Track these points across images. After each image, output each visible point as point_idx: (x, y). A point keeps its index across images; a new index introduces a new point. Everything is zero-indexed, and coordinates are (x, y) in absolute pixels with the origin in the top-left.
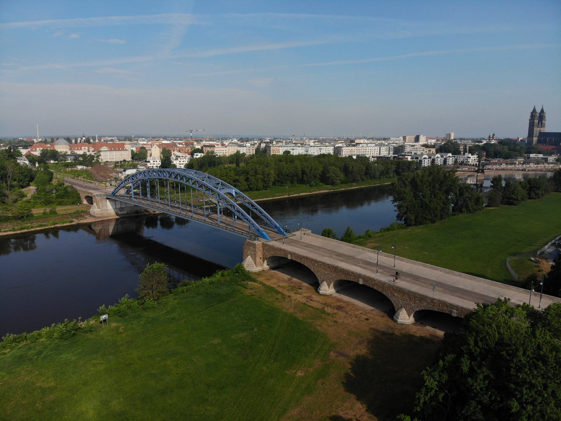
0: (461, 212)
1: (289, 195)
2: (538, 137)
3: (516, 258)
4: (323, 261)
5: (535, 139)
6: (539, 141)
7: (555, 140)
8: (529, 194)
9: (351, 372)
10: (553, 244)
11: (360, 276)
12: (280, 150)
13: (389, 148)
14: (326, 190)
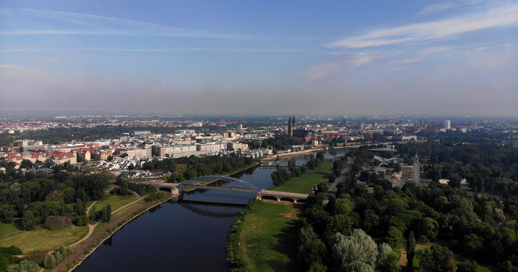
2: (293, 132)
4: (90, 235)
5: (292, 133)
6: (294, 135)
8: (302, 172)
10: (313, 188)
11: (286, 196)
12: (166, 150)
13: (225, 145)
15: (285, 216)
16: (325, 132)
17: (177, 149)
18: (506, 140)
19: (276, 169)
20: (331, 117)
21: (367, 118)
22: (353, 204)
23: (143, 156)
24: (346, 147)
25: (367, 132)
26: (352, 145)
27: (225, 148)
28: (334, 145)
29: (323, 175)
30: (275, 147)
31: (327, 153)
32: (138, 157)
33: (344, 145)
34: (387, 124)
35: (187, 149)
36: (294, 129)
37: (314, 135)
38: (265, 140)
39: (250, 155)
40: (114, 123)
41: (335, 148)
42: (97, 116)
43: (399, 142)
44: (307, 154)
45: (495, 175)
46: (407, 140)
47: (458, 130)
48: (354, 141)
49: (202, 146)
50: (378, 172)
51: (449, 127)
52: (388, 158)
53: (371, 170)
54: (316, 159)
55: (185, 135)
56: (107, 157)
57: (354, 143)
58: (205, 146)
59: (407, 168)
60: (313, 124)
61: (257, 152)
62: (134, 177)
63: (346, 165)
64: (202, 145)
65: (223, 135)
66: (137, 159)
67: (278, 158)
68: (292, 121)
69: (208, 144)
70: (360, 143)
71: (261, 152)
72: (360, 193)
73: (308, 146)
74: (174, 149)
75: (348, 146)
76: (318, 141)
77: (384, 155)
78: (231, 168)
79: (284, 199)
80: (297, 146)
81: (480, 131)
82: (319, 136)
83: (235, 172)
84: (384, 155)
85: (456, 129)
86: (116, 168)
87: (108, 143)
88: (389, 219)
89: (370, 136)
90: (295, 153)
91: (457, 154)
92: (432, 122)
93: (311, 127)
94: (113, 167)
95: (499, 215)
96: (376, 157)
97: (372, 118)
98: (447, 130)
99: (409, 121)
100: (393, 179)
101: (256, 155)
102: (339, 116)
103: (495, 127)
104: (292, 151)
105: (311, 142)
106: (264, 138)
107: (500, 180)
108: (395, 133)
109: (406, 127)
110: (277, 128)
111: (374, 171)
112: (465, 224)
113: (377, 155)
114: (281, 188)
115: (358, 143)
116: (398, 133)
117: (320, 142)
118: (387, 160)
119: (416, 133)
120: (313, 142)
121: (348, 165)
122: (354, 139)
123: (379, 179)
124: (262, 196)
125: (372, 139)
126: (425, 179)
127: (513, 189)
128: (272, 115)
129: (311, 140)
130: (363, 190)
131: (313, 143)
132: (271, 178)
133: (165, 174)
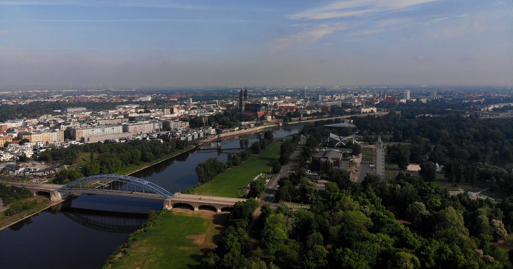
0: (219, 173)
1: (131, 173)
3: (240, 190)
5: (243, 108)
6: (246, 109)
7: (254, 108)
8: (242, 159)
9: (193, 240)
11: (207, 203)
12: (83, 132)
14: (147, 166)
15: (194, 242)
16: (282, 105)
17: (98, 131)
18: (469, 110)
19: (217, 152)
20: (292, 89)
21: (327, 88)
22: (292, 221)
23: (53, 140)
24: (302, 122)
25: (325, 105)
26: (308, 119)
27: (160, 127)
28: (288, 120)
29: (268, 162)
30: (221, 124)
31: (280, 129)
32: (41, 143)
33: (300, 120)
34: (345, 95)
35: (110, 131)
36: (246, 102)
37: (267, 109)
38: (211, 116)
39: (185, 136)
40: (54, 99)
41: (289, 123)
42: (43, 91)
43: (357, 115)
44: (258, 131)
45: (474, 158)
46: (366, 112)
47: (418, 100)
48: (310, 115)
49: (130, 126)
50: (332, 159)
51: (409, 98)
52: (346, 136)
53: (323, 157)
54: (263, 140)
55: (119, 112)
56: (3, 143)
57: (309, 117)
58: (134, 126)
59: (368, 148)
60: (271, 96)
61: (189, 134)
62: (17, 174)
63: (297, 146)
64: (131, 124)
65: (163, 111)
66: (39, 145)
67: (220, 139)
68: (243, 94)
69: (139, 122)
70: (316, 117)
71: (195, 134)
72: (308, 194)
73: (259, 122)
74: (93, 130)
75: (303, 120)
76: (271, 116)
77: (342, 132)
78: (153, 156)
79: (203, 207)
80: (247, 123)
81: (440, 101)
82: (274, 109)
83: (158, 161)
84: (342, 132)
85: (416, 99)
86: (6, 159)
87: (21, 124)
88: (343, 255)
89: (328, 108)
90: (243, 131)
91: (423, 129)
92: (390, 92)
93: (269, 99)
94: (3, 157)
95: (499, 229)
96: (332, 136)
97: (331, 89)
98: (407, 101)
99: (368, 91)
100: (351, 165)
101: (193, 136)
102: (301, 88)
103: (455, 97)
104: (240, 129)
105: (264, 117)
106: (211, 113)
107: (481, 166)
108: (354, 105)
109: (365, 98)
110: (232, 101)
111: (327, 158)
112: (462, 262)
113: (333, 133)
114: (208, 185)
115: (315, 117)
116: (356, 105)
117: (274, 117)
118: (345, 139)
119: (376, 104)
120: (265, 117)
121: (301, 146)
122: (311, 112)
123: (333, 168)
124: (174, 203)
125: (330, 112)
126: (390, 164)
127: (502, 181)
128: (233, 87)
129: (264, 115)
130: (311, 189)
131: (265, 119)
132: (196, 172)
133: (58, 169)
